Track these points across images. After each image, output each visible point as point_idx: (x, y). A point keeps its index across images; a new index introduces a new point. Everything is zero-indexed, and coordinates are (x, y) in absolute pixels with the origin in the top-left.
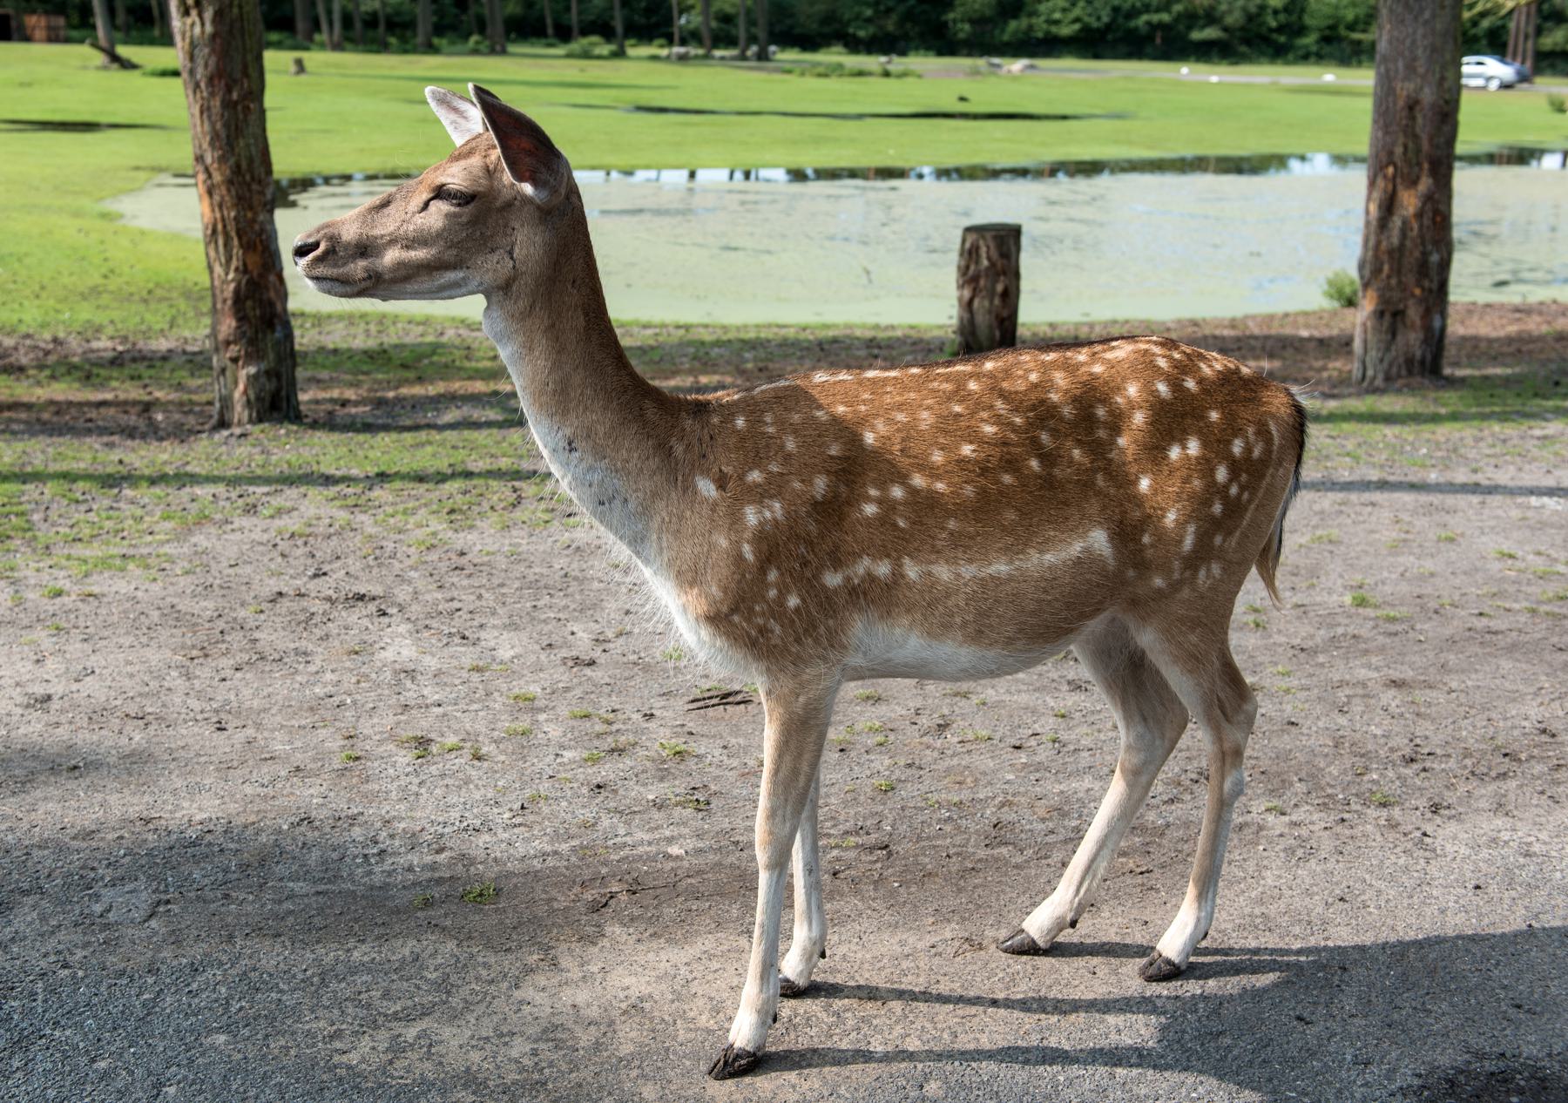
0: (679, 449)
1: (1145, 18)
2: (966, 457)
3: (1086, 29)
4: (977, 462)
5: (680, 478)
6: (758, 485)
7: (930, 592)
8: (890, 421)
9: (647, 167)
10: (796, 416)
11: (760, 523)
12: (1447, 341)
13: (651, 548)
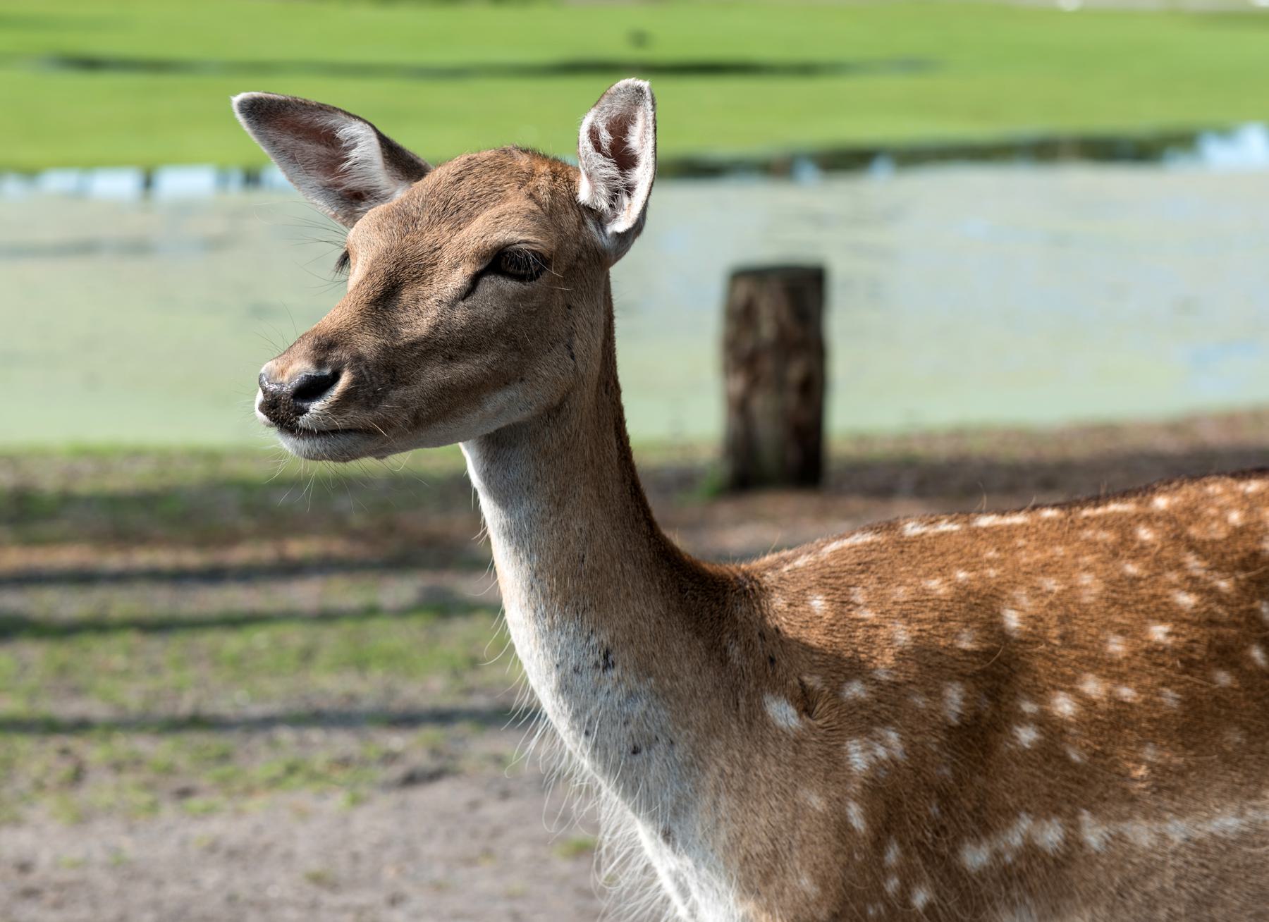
0: (735, 652)
2: (1158, 644)
4: (1175, 652)
5: (742, 701)
6: (862, 705)
7: (1122, 868)
8: (1036, 592)
9: (65, 164)
10: (901, 590)
11: (870, 764)
12: (644, 484)
13: (699, 821)
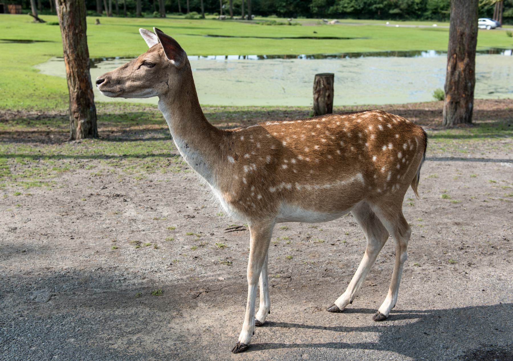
0: (222, 147)
1: (375, 6)
2: (316, 149)
3: (355, 10)
4: (320, 151)
5: (222, 156)
6: (248, 159)
7: (304, 194)
8: (291, 138)
9: (212, 55)
10: (261, 136)
11: (249, 171)
12: (473, 112)
13: (213, 179)
